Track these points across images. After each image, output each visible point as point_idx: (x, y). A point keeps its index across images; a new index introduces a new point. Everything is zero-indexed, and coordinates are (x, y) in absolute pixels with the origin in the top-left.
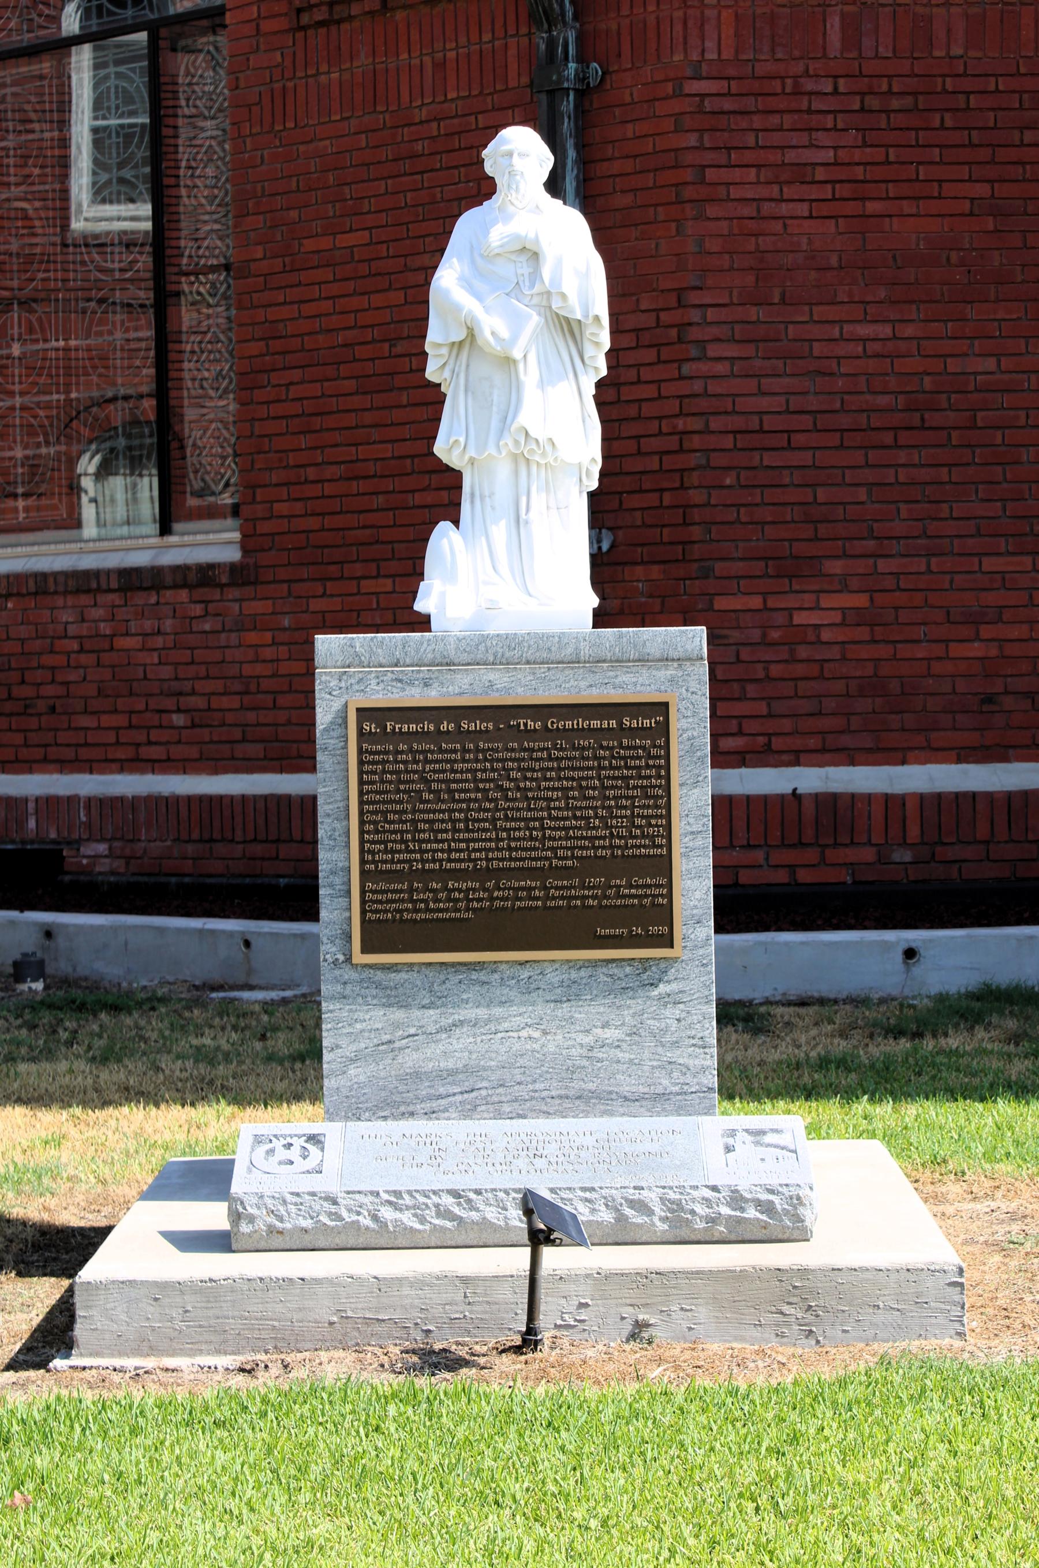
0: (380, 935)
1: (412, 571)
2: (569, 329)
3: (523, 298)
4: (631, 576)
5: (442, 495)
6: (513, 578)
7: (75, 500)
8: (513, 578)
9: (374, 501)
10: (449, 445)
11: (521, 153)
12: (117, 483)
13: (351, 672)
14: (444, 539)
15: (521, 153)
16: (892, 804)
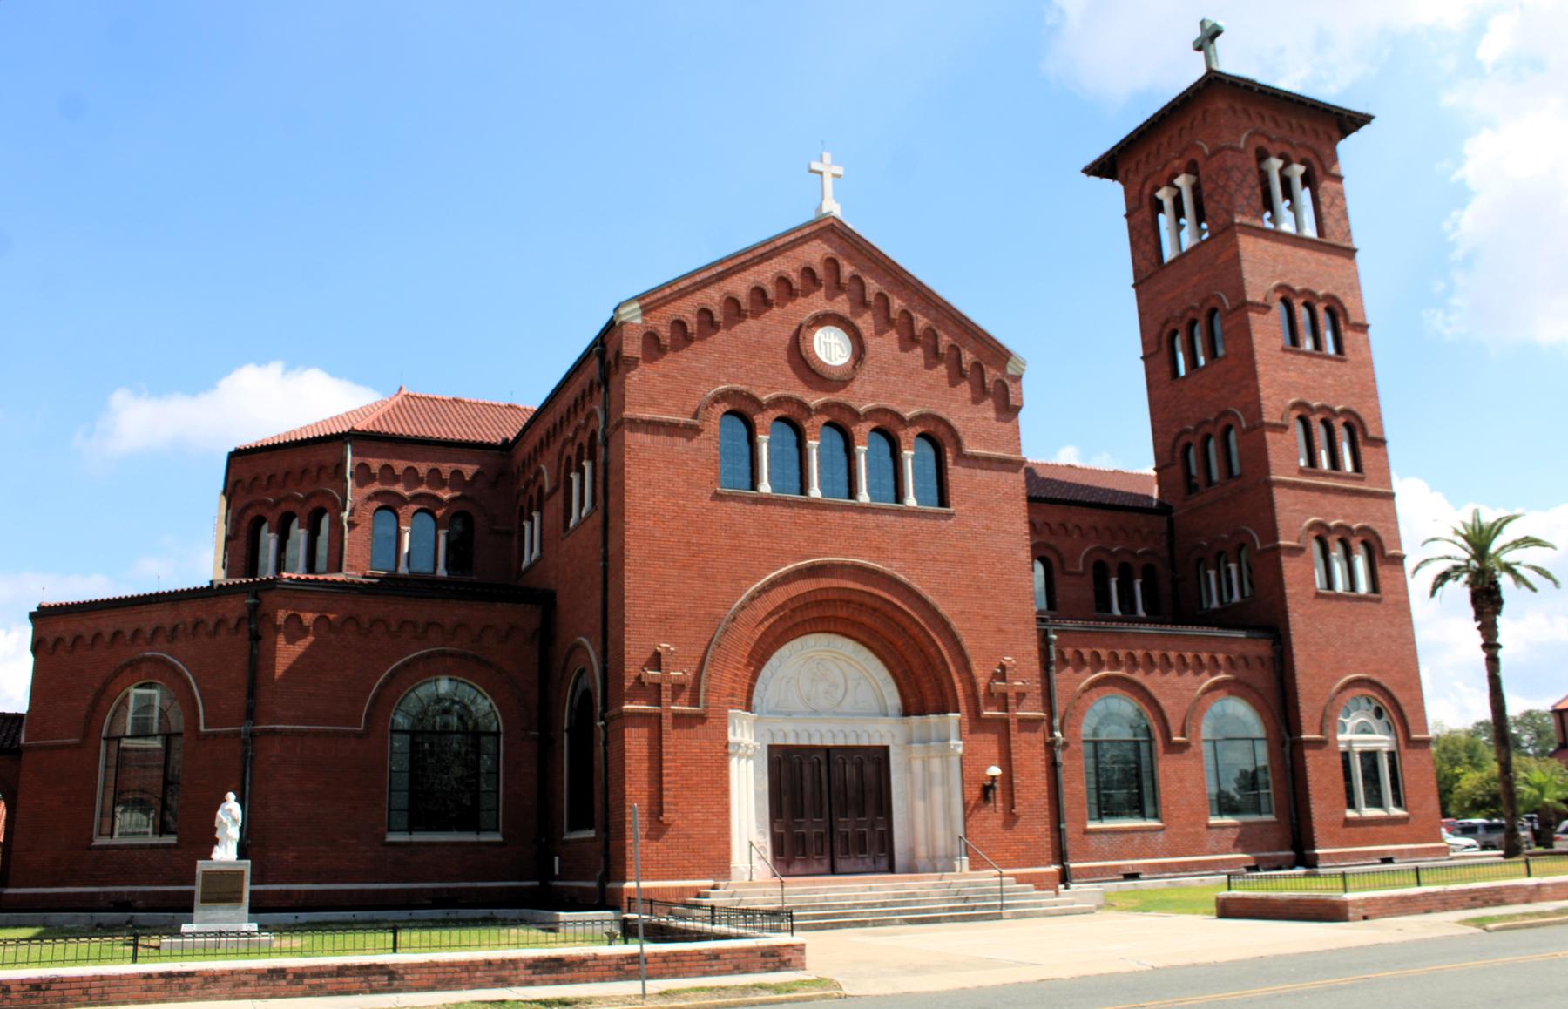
0: (203, 901)
1: (211, 852)
2: (235, 821)
3: (230, 814)
4: (243, 852)
5: (216, 842)
6: (226, 853)
7: (875, 645)
8: (226, 853)
9: (209, 841)
10: (218, 835)
11: (231, 796)
12: (127, 815)
13: (202, 866)
14: (216, 848)
15: (231, 796)
16: (299, 892)
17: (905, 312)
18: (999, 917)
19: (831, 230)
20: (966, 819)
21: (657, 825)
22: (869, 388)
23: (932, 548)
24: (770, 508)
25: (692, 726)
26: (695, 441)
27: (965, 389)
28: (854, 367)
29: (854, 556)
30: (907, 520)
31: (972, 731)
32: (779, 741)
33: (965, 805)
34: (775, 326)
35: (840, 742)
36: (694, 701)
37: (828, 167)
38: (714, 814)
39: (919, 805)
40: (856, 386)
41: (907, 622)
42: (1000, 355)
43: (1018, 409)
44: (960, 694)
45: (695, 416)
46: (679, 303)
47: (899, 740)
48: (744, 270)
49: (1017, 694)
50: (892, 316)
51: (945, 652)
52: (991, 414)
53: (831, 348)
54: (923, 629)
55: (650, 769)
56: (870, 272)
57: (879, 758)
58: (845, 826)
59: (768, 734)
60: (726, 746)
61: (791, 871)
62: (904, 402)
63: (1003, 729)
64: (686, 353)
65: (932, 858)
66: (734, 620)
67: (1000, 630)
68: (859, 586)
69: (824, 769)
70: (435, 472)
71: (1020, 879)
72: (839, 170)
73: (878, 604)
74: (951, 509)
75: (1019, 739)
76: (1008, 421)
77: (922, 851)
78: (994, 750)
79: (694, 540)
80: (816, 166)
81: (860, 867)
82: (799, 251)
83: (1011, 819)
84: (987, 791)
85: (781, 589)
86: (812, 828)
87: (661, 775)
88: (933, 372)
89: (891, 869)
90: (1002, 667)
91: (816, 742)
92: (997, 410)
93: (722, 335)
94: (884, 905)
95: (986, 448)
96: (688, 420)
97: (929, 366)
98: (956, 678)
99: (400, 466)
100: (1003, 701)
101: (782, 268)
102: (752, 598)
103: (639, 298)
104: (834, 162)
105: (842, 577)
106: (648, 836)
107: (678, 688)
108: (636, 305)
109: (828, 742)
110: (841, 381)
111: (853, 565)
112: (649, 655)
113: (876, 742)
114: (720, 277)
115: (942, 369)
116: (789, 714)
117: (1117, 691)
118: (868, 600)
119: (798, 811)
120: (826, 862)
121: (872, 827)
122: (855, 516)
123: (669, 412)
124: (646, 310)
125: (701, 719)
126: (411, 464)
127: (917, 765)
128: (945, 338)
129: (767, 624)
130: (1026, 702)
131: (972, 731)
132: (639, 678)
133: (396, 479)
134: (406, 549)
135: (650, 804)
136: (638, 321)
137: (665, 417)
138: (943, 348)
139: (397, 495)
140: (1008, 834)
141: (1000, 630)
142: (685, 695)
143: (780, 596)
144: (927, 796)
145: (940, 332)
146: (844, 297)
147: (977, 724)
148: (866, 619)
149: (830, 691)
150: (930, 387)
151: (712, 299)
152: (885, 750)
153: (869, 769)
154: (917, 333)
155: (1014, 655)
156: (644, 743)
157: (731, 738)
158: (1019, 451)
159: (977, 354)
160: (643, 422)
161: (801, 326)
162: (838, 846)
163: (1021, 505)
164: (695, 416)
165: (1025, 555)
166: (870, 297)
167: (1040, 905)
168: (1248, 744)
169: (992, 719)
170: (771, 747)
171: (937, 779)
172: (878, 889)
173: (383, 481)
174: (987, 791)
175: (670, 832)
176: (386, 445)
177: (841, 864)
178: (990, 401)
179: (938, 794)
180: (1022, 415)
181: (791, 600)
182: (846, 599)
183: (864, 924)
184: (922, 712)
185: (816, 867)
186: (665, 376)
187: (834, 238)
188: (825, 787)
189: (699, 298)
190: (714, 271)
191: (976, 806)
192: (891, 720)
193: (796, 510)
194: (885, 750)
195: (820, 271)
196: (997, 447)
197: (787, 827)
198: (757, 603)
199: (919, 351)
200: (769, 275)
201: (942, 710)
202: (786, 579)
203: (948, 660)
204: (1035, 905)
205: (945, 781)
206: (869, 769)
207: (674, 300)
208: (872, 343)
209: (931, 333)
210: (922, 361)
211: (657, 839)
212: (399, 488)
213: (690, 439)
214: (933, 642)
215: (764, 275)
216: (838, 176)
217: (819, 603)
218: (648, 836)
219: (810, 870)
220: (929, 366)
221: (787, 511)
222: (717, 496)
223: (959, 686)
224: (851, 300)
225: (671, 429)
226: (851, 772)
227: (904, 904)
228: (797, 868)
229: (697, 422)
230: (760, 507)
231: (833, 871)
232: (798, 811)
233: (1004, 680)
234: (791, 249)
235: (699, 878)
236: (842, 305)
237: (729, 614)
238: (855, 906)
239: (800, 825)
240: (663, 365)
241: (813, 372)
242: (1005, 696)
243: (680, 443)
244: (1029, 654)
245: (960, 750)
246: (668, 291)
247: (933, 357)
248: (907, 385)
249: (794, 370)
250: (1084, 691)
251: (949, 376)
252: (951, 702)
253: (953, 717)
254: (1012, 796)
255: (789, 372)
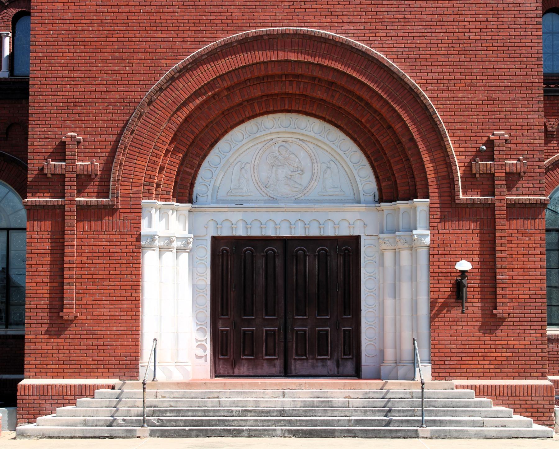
18: (415, 435)
20: (432, 319)
25: (100, 218)
29: (299, 24)
31: (443, 219)
32: (226, 232)
33: (432, 304)
35: (299, 232)
36: (104, 192)
39: (389, 302)
41: (366, 96)
44: (431, 176)
47: (371, 230)
57: (347, 250)
58: (303, 324)
59: (212, 225)
60: (138, 238)
61: (236, 372)
63: (485, 216)
65: (397, 362)
71: (481, 392)
73: (330, 77)
75: (506, 229)
78: (474, 241)
79: (108, 20)
81: (320, 370)
83: (491, 322)
85: (208, 67)
86: (261, 325)
87: (62, 269)
89: (357, 374)
90: (490, 144)
94: (281, 413)
98: (426, 158)
100: (487, 182)
102: (172, 79)
106: (47, 332)
107: (83, 181)
109: (285, 232)
111: (296, 34)
113: (344, 232)
118: (318, 73)
119: (246, 308)
120: (279, 363)
125: (111, 210)
129: (192, 106)
130: (522, 184)
131: (443, 219)
134: (7, 52)
135: (51, 299)
142: (94, 186)
143: (206, 74)
144: (396, 293)
147: (449, 210)
153: (336, 262)
156: (47, 235)
157: (145, 230)
169: (472, 205)
170: (215, 240)
171: (406, 274)
175: (72, 328)
177: (296, 366)
179: (405, 289)
184: (392, 199)
188: (281, 282)
191: (444, 305)
198: (179, 84)
201: (410, 196)
203: (417, 138)
205: (413, 278)
206: (336, 262)
211: (58, 334)
214: (399, 116)
217: (261, 80)
218: (47, 332)
219: (259, 372)
223: (429, 167)
228: (244, 370)
232: (246, 308)
235: (103, 377)
237: (145, 97)
239: (249, 322)
245: (427, 241)
253: (422, 204)
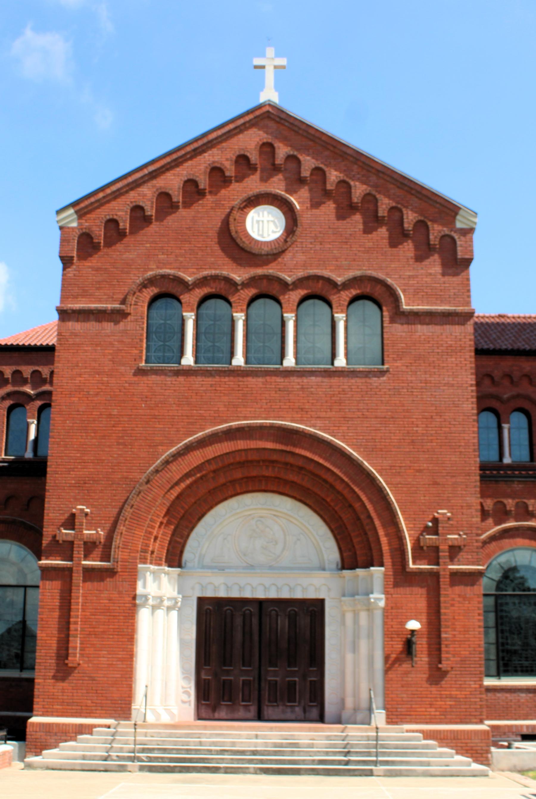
17: (342, 183)
18: (370, 773)
19: (270, 118)
20: (386, 671)
21: (64, 670)
22: (301, 257)
23: (361, 406)
24: (192, 379)
25: (102, 579)
26: (122, 324)
27: (408, 249)
28: (286, 241)
29: (275, 418)
30: (335, 380)
31: (396, 585)
32: (209, 594)
33: (387, 658)
34: (206, 215)
36: (106, 557)
37: (270, 59)
38: (120, 660)
39: (349, 657)
40: (287, 257)
41: (331, 479)
42: (447, 210)
43: (468, 262)
44: (385, 548)
45: (123, 302)
46: (113, 204)
48: (177, 166)
49: (451, 547)
50: (329, 187)
51: (369, 507)
52: (437, 269)
53: (264, 225)
54: (347, 485)
55: (60, 617)
56: (306, 150)
57: (314, 609)
58: (275, 674)
59: (198, 587)
60: (134, 598)
61: (216, 715)
62: (339, 268)
63: (431, 582)
64: (119, 246)
65: (356, 709)
66: (148, 482)
67: (436, 483)
68: (278, 447)
69: (255, 621)
70: (17, 373)
71: (428, 735)
72: (282, 62)
73: (300, 463)
74: (386, 367)
75: (450, 594)
76: (456, 274)
77: (349, 703)
78: (422, 604)
79: (115, 412)
80: (257, 62)
81: (289, 715)
82: (234, 140)
83: (437, 674)
84: (409, 645)
86: (239, 675)
87: (68, 623)
88: (374, 235)
89: (321, 719)
90: (435, 521)
91: (248, 594)
92: (445, 265)
93: (154, 227)
94: (254, 753)
95: (428, 304)
96: (117, 306)
97: (368, 230)
98: (381, 532)
99: (27, 371)
101: (216, 159)
102: (167, 462)
103: (73, 205)
104: (263, 55)
105: (261, 439)
106: (54, 677)
107: (90, 547)
108: (71, 211)
109: (260, 595)
110: (275, 253)
111: (272, 427)
112: (67, 515)
114: (154, 175)
115: (383, 231)
116: (222, 569)
117: (520, 541)
119: (225, 660)
120: (253, 709)
121: (304, 677)
122: (279, 380)
123: (100, 301)
124: (81, 214)
125: (111, 573)
126: (37, 368)
127: (349, 617)
128: (386, 201)
129: (183, 485)
130: (462, 555)
131: (396, 585)
132: (54, 537)
133: (25, 382)
135: (59, 649)
136: (75, 225)
137: (93, 306)
138: (382, 212)
139: (25, 394)
140: (434, 689)
141: (436, 483)
142: (98, 552)
143: (196, 458)
145: (379, 197)
146: (280, 176)
147: (401, 577)
148: (292, 477)
149: (264, 546)
150: (368, 251)
151: (144, 195)
152: (321, 603)
153: (304, 622)
154: (355, 200)
155: (450, 508)
156: (57, 593)
157: (140, 590)
158: (468, 303)
159: (421, 212)
160: (74, 311)
161: (232, 209)
162: (266, 694)
163: (469, 356)
164: (123, 302)
165: (469, 406)
166: (306, 173)
167: (428, 764)
168: (23, 589)
171: (364, 632)
172: (265, 737)
173: (14, 384)
174: (409, 645)
175: (76, 674)
176: (16, 354)
177: (268, 711)
178: (436, 257)
180: (473, 268)
181: (208, 461)
182: (265, 459)
183: (216, 770)
184: (353, 567)
185: (241, 713)
186: (97, 269)
187: (271, 124)
188: (256, 638)
189: (133, 197)
190: (146, 171)
192: (327, 574)
193: (217, 379)
194: (321, 603)
195: (254, 157)
196: (442, 302)
197: (216, 675)
198: (173, 467)
199: (358, 217)
200: (202, 167)
201: (368, 565)
202: (202, 443)
204: (421, 764)
206: (304, 622)
207: (108, 202)
208: (306, 216)
209: (370, 199)
210: (361, 227)
212: (29, 390)
213: (117, 322)
214: (358, 497)
215: (198, 168)
216: (283, 67)
217: (242, 464)
218: (54, 677)
220: (368, 230)
221: (209, 380)
222: (140, 372)
223: (384, 540)
224: (286, 179)
225: (100, 315)
226: (283, 623)
227: (276, 753)
229: (123, 307)
230: (181, 379)
231: (260, 717)
232: (225, 660)
233: (436, 533)
234: (226, 140)
236: (277, 186)
237: (143, 478)
238: (223, 752)
239: (228, 673)
240: (95, 261)
241: (242, 249)
242: (436, 549)
243: (108, 327)
244: (469, 507)
245: (382, 604)
246: (101, 195)
247: (373, 221)
248: (350, 251)
249: (223, 250)
250: (485, 543)
251: (390, 237)
252: (375, 554)
253: (377, 571)
254: (439, 650)
255: (219, 252)
